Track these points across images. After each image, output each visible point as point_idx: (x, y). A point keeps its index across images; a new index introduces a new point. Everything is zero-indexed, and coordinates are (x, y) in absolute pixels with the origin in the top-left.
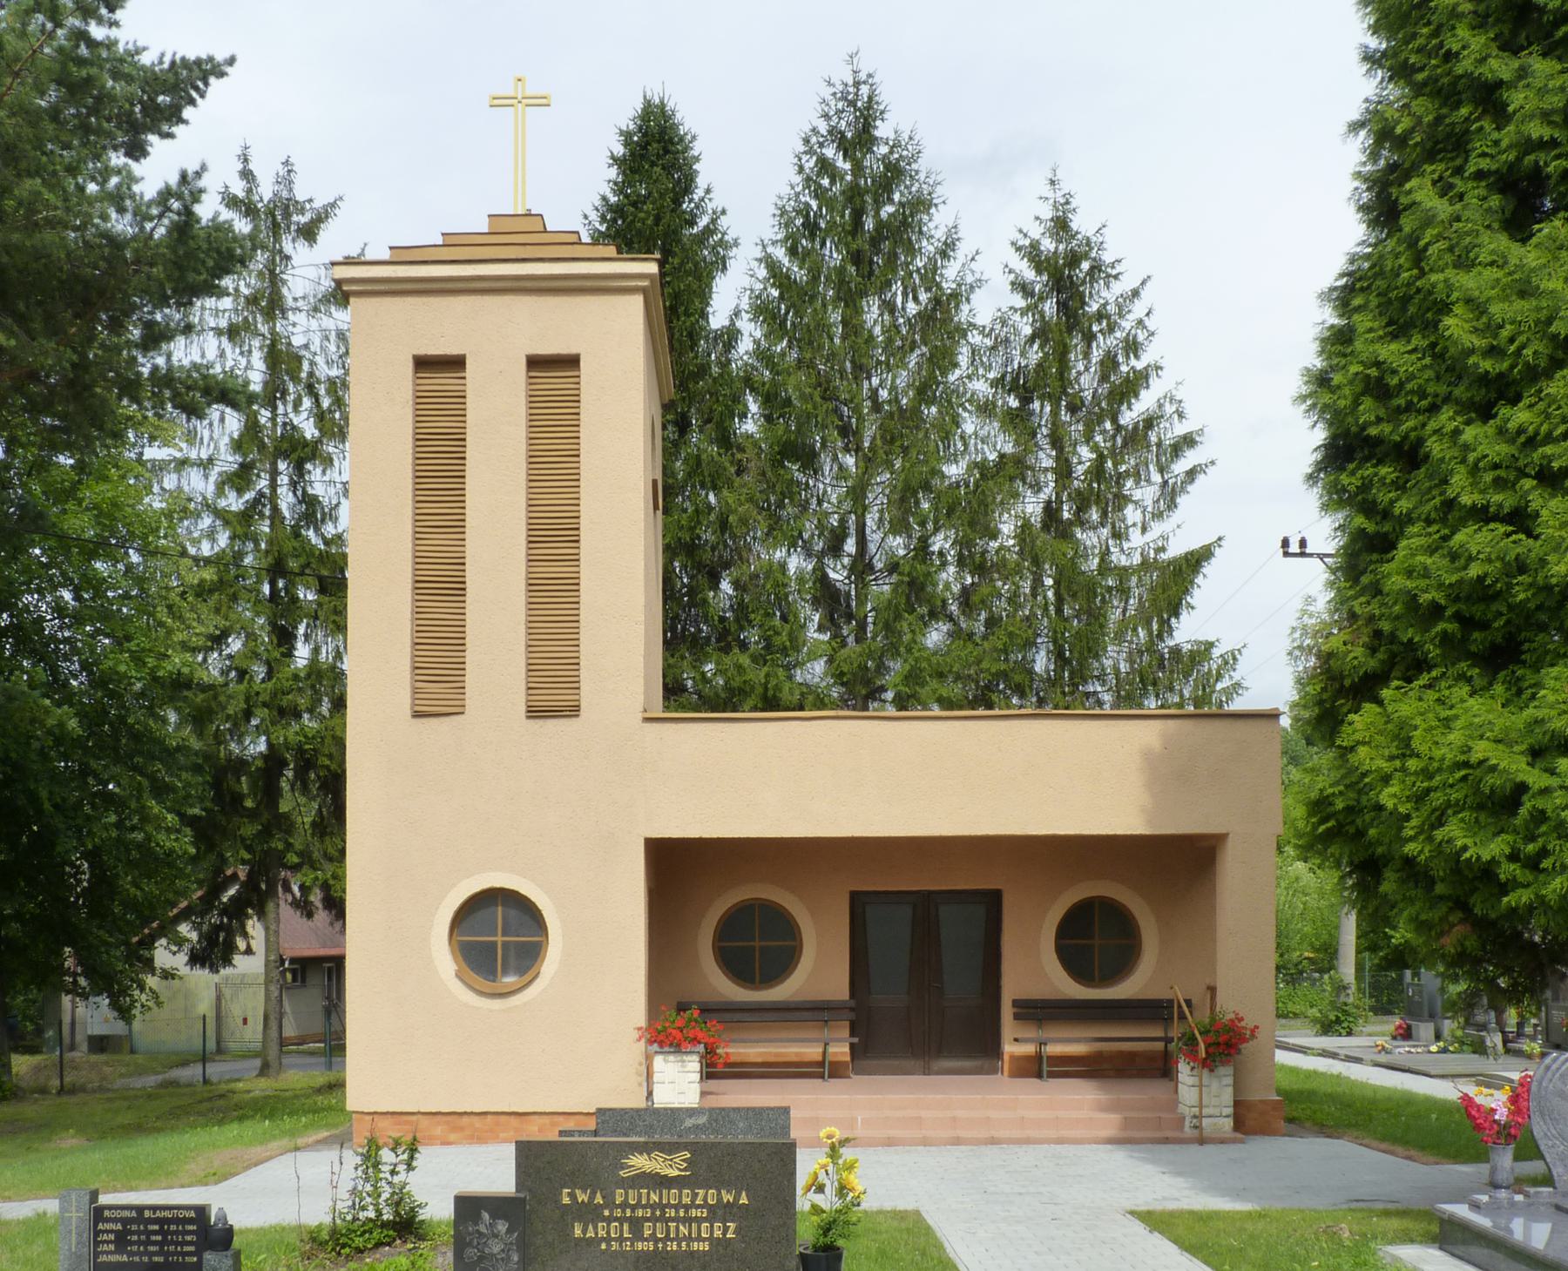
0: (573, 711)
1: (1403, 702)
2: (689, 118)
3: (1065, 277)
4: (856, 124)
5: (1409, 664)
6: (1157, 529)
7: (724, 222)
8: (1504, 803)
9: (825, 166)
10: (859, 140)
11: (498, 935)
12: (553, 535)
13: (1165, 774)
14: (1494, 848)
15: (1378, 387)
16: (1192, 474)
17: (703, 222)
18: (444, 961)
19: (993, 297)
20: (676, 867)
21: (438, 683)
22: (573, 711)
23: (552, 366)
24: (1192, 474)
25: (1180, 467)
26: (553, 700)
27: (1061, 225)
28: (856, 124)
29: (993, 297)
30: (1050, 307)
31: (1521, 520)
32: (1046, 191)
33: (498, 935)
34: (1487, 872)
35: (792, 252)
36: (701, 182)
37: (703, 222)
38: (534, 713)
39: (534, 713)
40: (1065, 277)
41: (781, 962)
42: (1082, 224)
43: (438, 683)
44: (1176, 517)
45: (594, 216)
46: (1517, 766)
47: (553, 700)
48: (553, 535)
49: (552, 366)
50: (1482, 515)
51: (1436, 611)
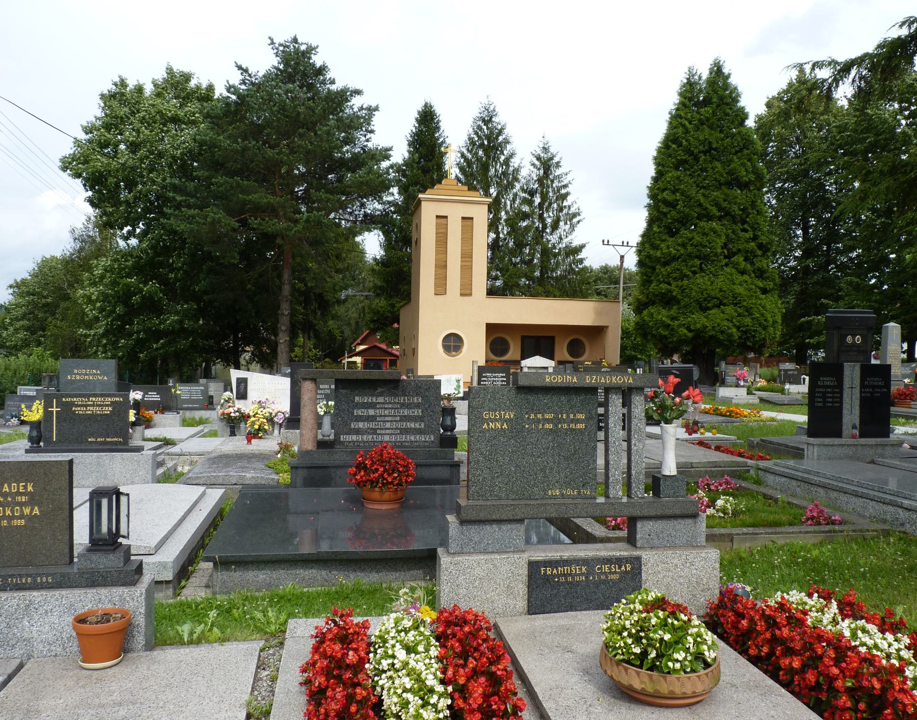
0: (470, 295)
1: (652, 309)
2: (438, 109)
3: (546, 164)
4: (487, 119)
5: (653, 303)
6: (570, 237)
7: (447, 140)
8: (667, 326)
9: (479, 127)
10: (487, 121)
11: (453, 343)
12: (467, 256)
13: (598, 313)
14: (666, 333)
15: (649, 256)
16: (578, 222)
17: (441, 140)
18: (465, 349)
19: (527, 171)
20: (491, 328)
21: (441, 288)
22: (470, 295)
23: (467, 220)
24: (578, 222)
25: (575, 220)
26: (466, 291)
27: (545, 149)
28: (487, 119)
29: (527, 171)
30: (542, 172)
31: (669, 284)
32: (542, 139)
33: (453, 343)
34: (665, 336)
35: (468, 150)
36: (442, 129)
37: (441, 140)
38: (462, 295)
39: (462, 295)
40: (546, 164)
41: (505, 351)
42: (553, 150)
43: (441, 288)
44: (574, 234)
45: (408, 136)
46: (669, 322)
47: (466, 291)
48: (467, 256)
49: (467, 220)
50: (664, 282)
51: (657, 295)
